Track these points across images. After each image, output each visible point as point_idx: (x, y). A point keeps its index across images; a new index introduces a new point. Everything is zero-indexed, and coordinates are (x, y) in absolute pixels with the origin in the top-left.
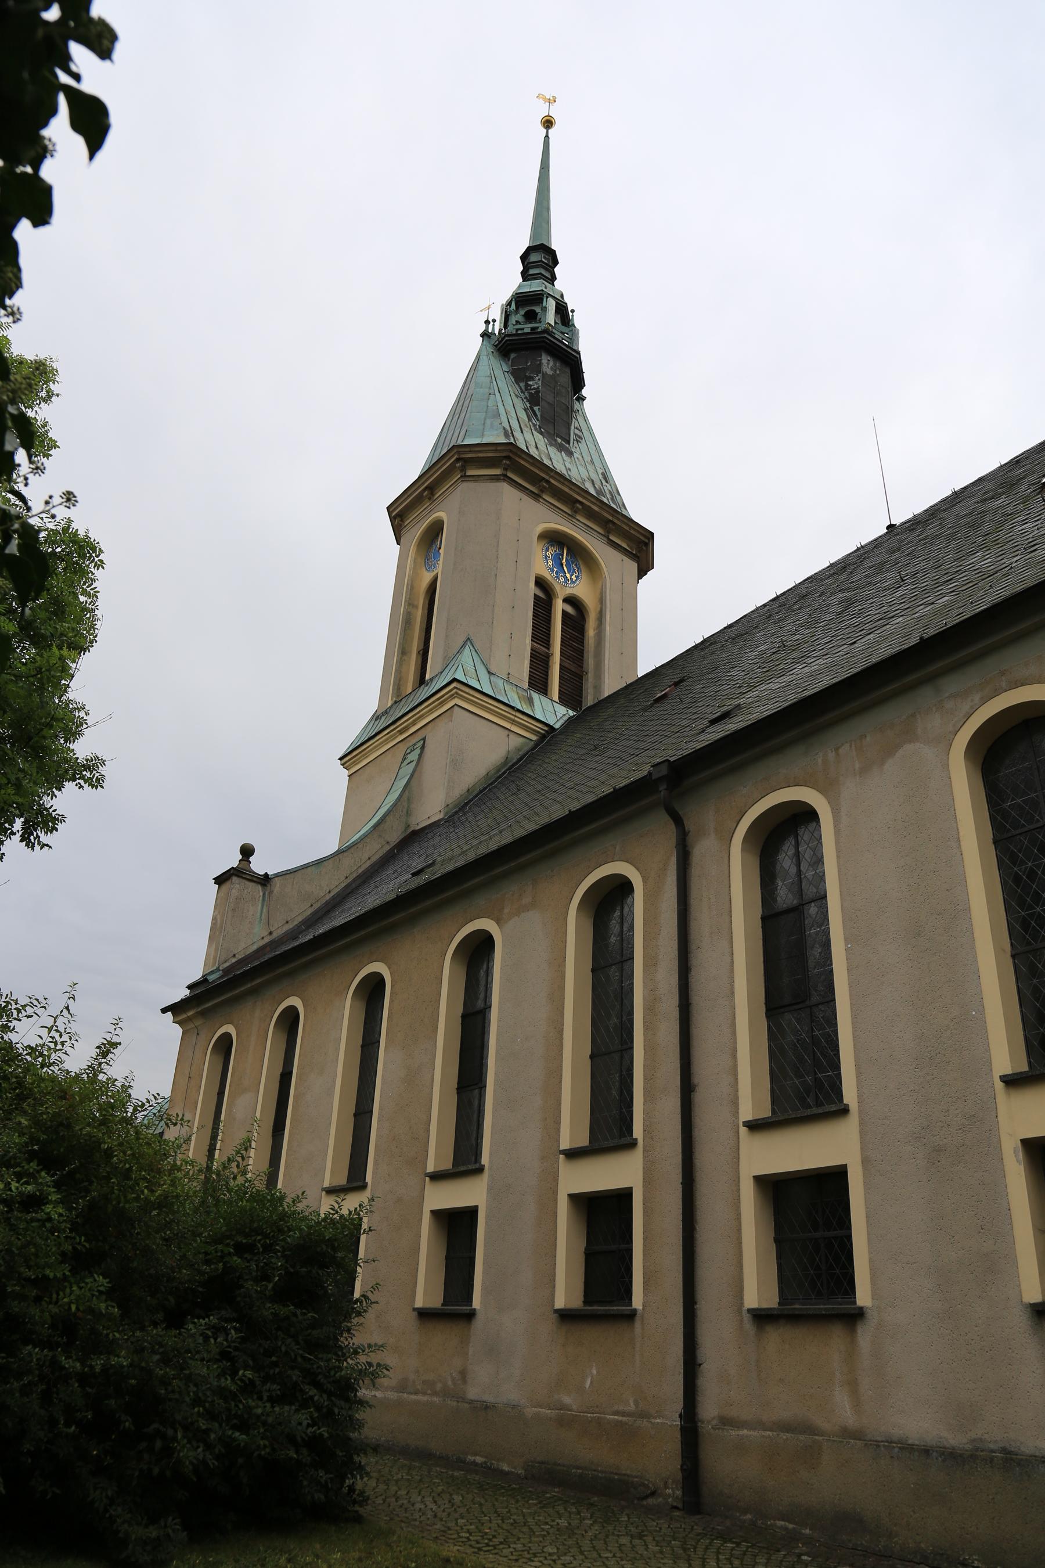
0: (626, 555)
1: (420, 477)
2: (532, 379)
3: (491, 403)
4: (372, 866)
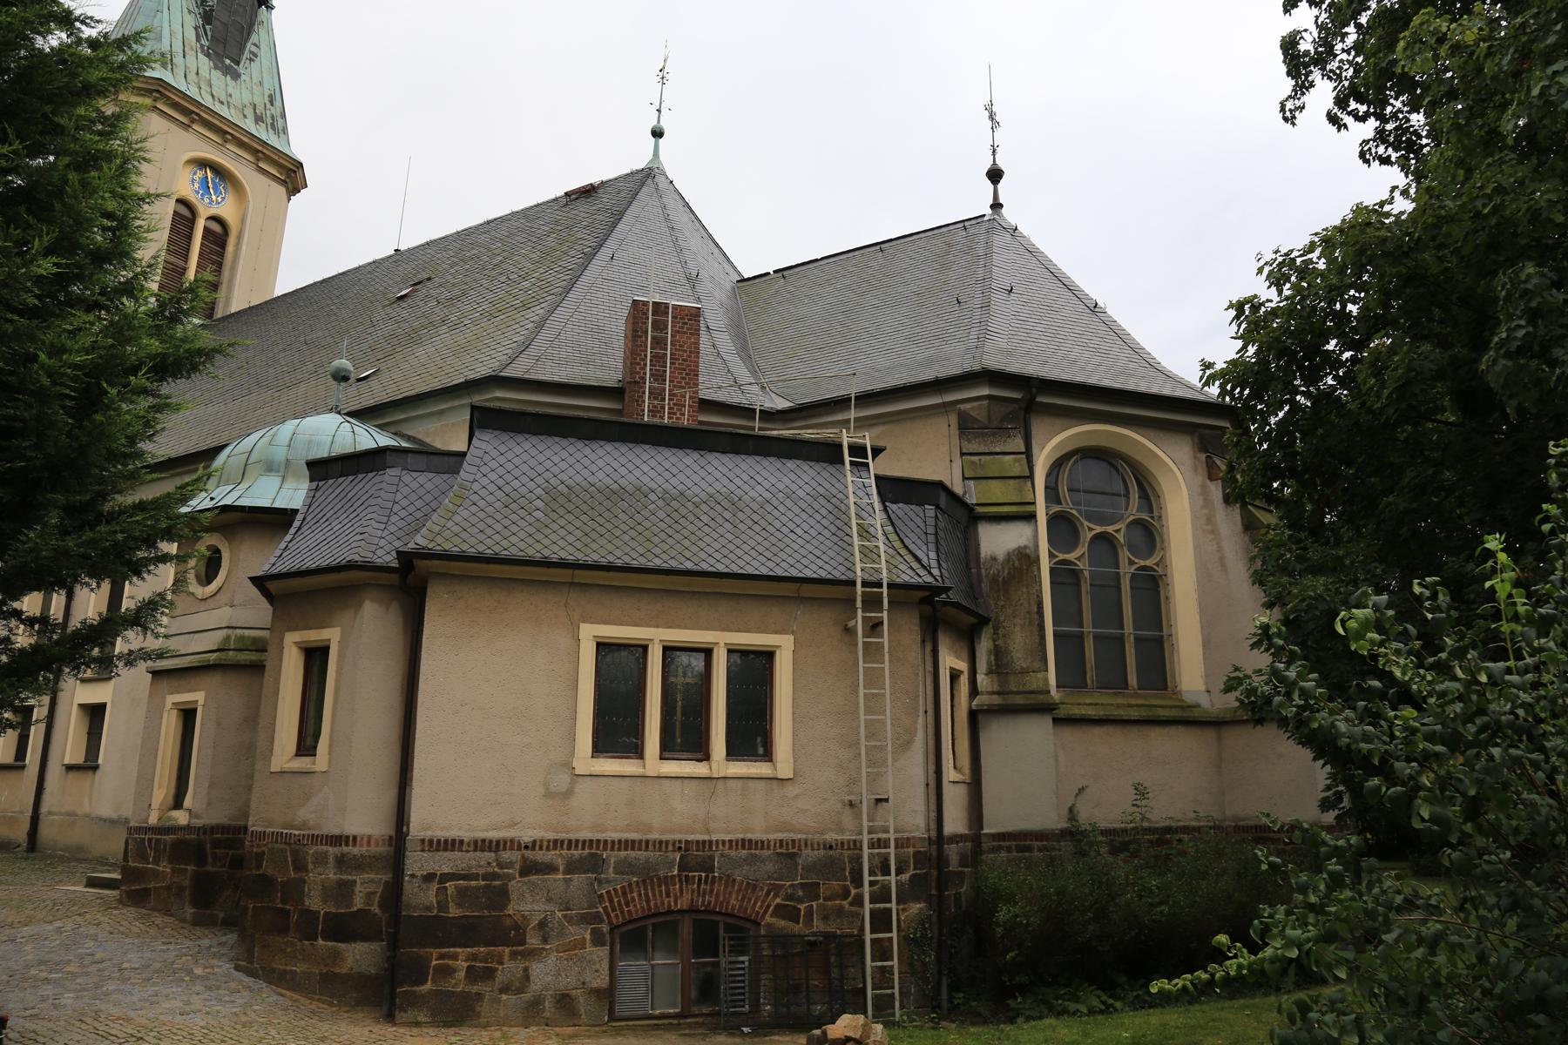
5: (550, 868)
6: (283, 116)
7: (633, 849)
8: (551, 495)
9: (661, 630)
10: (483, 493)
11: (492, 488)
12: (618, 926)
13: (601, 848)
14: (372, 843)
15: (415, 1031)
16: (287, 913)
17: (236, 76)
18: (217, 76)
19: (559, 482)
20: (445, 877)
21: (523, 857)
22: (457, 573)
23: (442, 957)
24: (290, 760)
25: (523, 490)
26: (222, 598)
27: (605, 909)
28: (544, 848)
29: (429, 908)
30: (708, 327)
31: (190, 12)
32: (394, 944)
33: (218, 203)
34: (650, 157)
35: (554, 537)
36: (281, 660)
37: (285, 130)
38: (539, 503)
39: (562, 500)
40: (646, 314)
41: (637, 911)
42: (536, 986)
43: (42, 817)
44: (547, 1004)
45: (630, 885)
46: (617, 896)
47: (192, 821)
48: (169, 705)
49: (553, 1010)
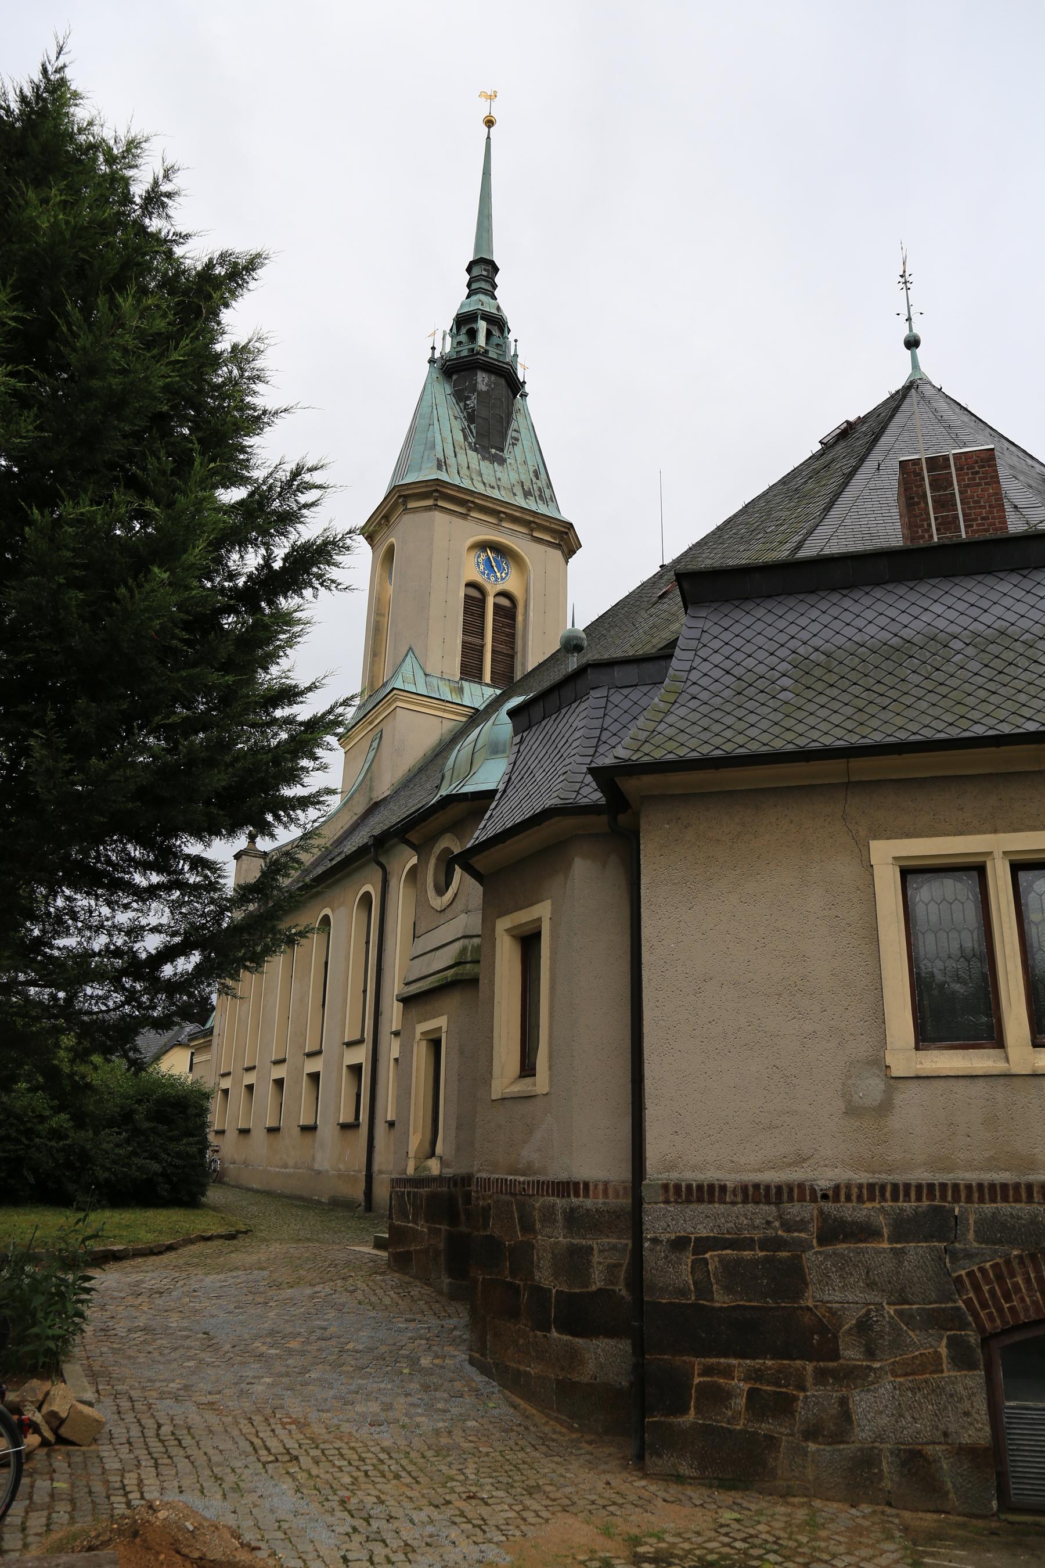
0: (549, 546)
1: (385, 499)
2: (469, 398)
3: (430, 434)
4: (344, 833)
5: (866, 1232)
6: (549, 485)
7: (1005, 1199)
8: (803, 667)
9: (1001, 836)
10: (705, 682)
11: (717, 673)
12: (995, 1336)
13: (949, 1198)
14: (610, 1192)
15: (674, 1489)
16: (517, 1290)
17: (502, 461)
18: (486, 467)
19: (811, 650)
20: (704, 1244)
21: (821, 1212)
22: (676, 792)
23: (707, 1371)
24: (513, 1083)
25: (761, 669)
26: (459, 905)
27: (968, 1302)
28: (854, 1197)
29: (683, 1292)
30: (1016, 507)
31: (456, 418)
32: (639, 1349)
33: (502, 579)
34: (910, 371)
35: (812, 721)
36: (494, 955)
37: (553, 498)
38: (786, 682)
39: (818, 672)
40: (920, 474)
41: (1026, 1310)
42: (863, 1433)
43: (374, 1175)
44: (885, 1466)
45: (1008, 1262)
46: (988, 1282)
47: (445, 1170)
48: (418, 1036)
49: (896, 1479)
